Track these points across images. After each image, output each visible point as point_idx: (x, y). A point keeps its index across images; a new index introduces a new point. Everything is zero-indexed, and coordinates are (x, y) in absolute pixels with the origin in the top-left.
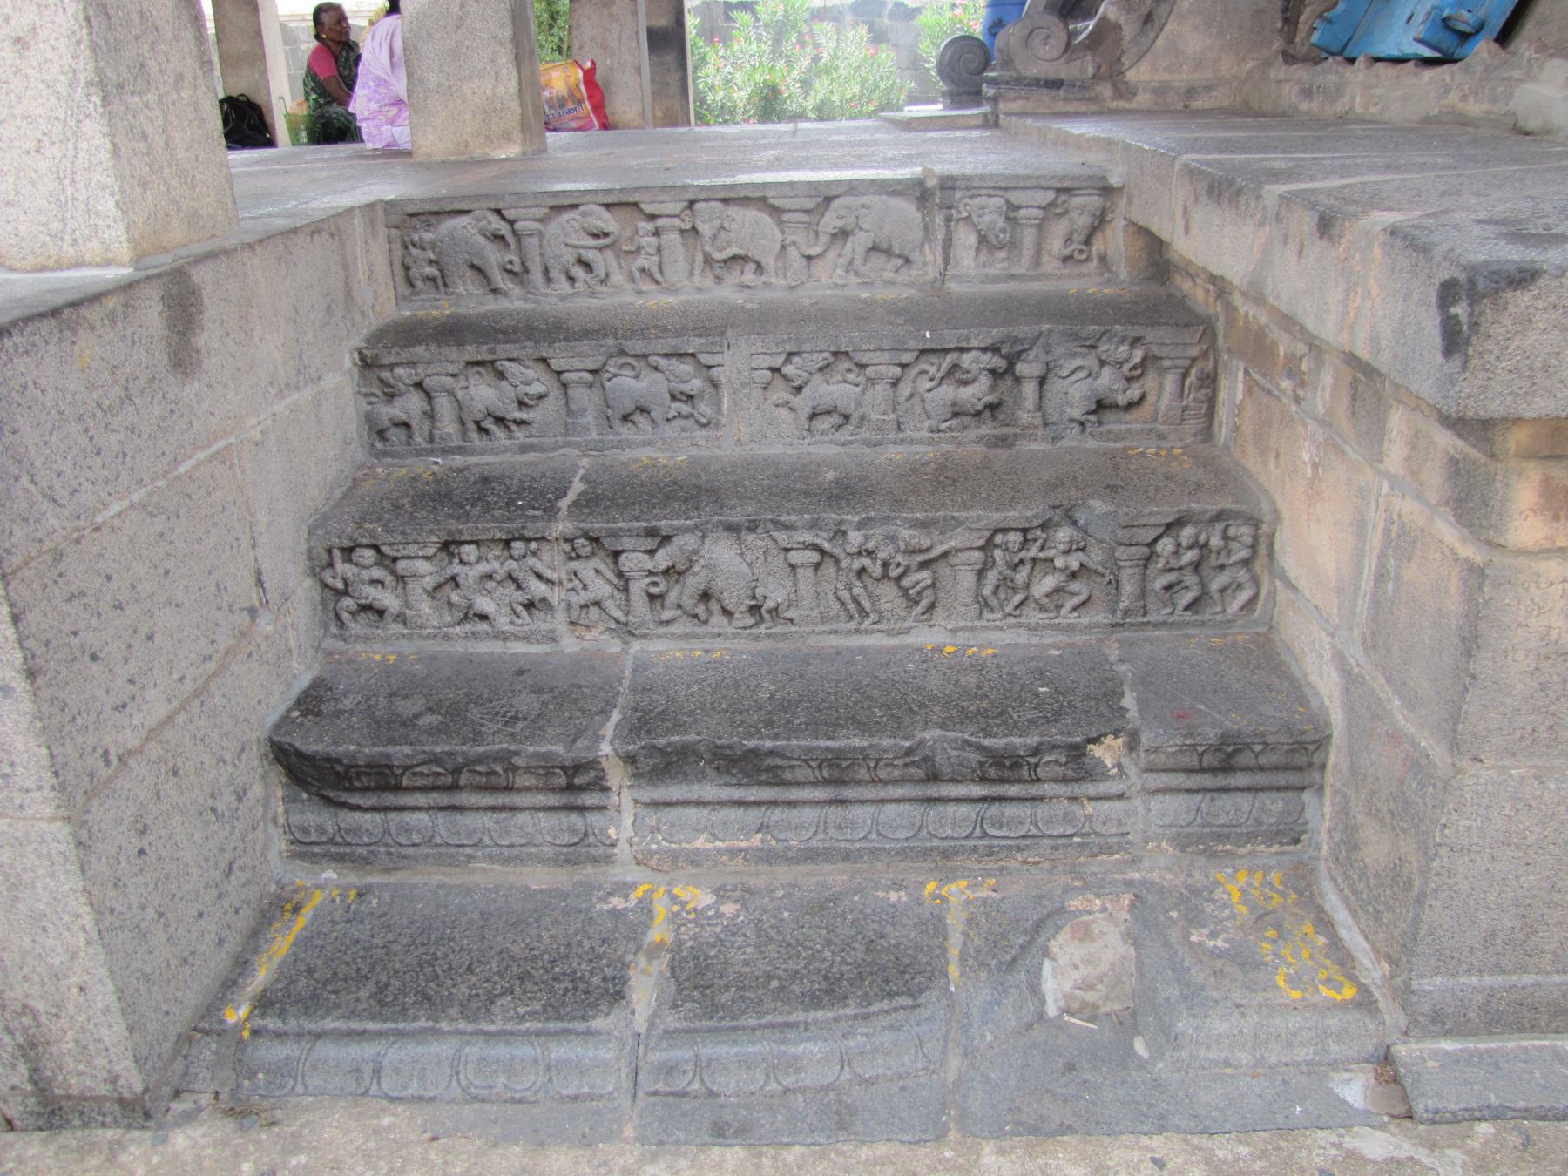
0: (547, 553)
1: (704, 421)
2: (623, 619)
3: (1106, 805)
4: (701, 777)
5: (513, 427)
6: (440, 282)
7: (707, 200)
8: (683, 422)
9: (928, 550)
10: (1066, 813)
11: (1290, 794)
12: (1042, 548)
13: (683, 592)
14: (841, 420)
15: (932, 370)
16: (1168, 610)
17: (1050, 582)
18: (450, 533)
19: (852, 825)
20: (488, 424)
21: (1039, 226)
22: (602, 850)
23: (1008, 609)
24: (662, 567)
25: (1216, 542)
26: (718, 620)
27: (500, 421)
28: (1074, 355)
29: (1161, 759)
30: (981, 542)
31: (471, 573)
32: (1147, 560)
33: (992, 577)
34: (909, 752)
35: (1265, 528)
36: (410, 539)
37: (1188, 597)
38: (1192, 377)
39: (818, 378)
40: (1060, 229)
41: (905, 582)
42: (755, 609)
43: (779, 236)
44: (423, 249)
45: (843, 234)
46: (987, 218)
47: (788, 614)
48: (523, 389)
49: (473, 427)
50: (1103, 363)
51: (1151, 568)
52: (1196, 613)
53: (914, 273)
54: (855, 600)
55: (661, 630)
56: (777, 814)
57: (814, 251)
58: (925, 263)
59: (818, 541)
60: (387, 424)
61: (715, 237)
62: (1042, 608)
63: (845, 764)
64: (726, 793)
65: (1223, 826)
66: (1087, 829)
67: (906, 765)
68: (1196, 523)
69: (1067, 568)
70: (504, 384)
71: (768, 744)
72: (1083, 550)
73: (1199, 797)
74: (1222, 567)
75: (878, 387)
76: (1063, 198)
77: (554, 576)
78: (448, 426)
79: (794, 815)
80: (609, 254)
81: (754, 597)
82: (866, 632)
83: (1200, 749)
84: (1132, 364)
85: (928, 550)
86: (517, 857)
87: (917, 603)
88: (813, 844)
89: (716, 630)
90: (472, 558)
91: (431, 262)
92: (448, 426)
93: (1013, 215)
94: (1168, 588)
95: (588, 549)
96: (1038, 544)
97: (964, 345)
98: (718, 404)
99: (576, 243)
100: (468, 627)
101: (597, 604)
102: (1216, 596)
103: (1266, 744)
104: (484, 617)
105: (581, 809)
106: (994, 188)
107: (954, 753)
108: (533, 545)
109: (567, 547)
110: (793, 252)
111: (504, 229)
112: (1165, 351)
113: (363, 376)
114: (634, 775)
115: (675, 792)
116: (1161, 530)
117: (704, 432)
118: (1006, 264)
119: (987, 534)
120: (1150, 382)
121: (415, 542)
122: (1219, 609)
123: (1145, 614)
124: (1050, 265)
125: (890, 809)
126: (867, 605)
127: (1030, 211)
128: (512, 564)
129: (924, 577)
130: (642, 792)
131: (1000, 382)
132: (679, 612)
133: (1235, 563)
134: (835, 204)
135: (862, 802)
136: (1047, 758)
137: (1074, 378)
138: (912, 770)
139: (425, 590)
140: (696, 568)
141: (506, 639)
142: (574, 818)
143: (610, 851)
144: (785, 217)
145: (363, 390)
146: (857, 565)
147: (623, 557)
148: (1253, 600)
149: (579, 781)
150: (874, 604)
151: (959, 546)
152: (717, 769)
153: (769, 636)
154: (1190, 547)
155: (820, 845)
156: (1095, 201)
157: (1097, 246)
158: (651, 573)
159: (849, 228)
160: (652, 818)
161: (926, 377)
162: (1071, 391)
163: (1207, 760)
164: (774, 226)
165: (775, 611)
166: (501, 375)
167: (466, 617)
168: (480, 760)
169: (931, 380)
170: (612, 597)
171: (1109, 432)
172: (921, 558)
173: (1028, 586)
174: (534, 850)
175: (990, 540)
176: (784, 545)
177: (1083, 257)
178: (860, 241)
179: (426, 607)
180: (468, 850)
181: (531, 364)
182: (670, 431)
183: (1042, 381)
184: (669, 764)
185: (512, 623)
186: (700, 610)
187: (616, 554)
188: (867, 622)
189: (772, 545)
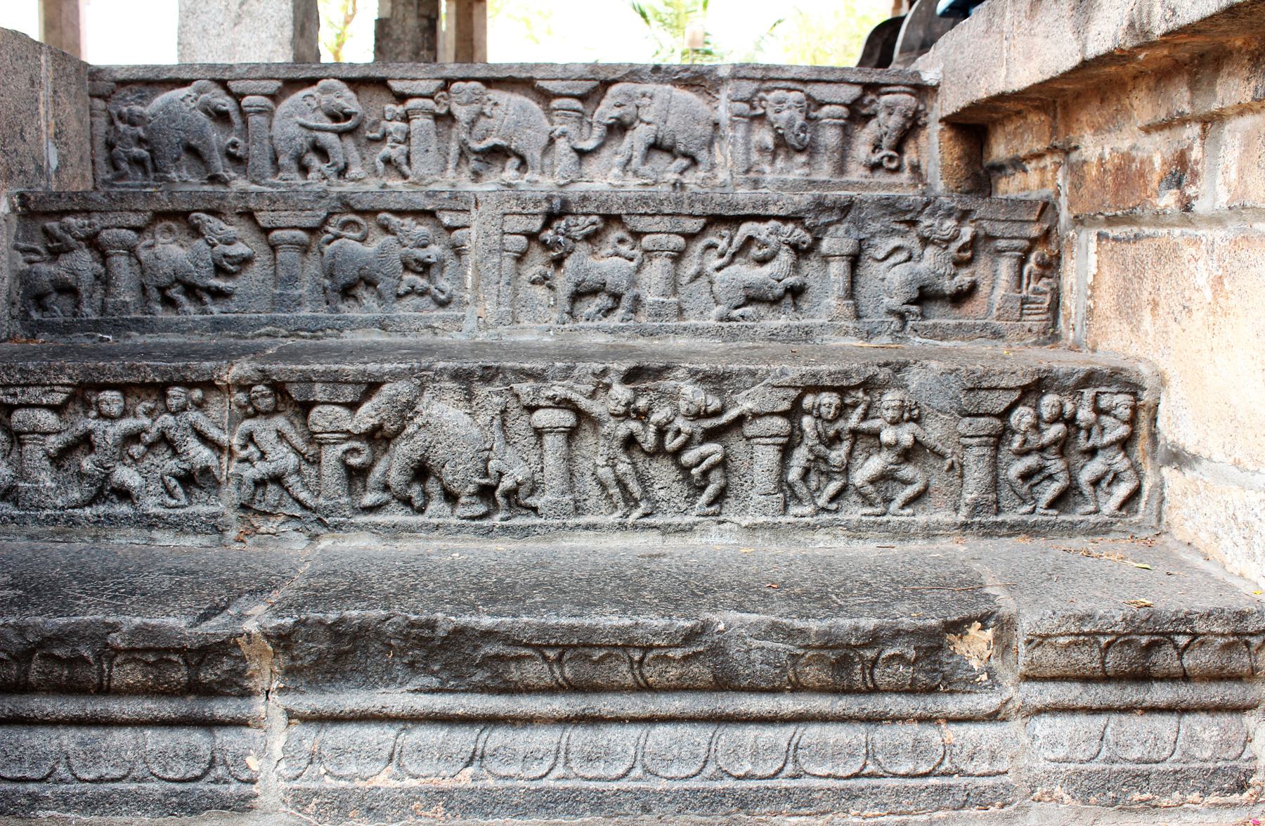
0: (219, 408)
1: (442, 297)
2: (311, 502)
3: (973, 731)
4: (388, 678)
5: (207, 299)
6: (149, 166)
7: (466, 80)
8: (415, 300)
9: (717, 413)
10: (917, 741)
11: (1225, 719)
12: (865, 417)
13: (392, 466)
14: (609, 303)
15: (722, 244)
16: (1027, 508)
17: (875, 464)
18: (86, 372)
19: (607, 755)
20: (174, 293)
21: (844, 127)
22: (233, 787)
23: (822, 502)
24: (363, 427)
25: (1085, 415)
26: (436, 506)
27: (192, 291)
28: (891, 233)
29: (1049, 658)
30: (785, 406)
31: (111, 430)
32: (999, 439)
33: (800, 456)
34: (691, 636)
35: (1146, 397)
36: (32, 380)
37: (1051, 490)
38: (1031, 265)
39: (582, 248)
40: (865, 136)
41: (688, 457)
42: (486, 493)
43: (547, 126)
44: (133, 124)
45: (618, 128)
46: (785, 114)
47: (531, 501)
48: (221, 248)
49: (155, 294)
50: (925, 241)
51: (1004, 449)
52: (1062, 512)
53: (701, 174)
54: (621, 483)
55: (361, 519)
56: (498, 737)
57: (589, 145)
58: (713, 166)
59: (574, 396)
60: (49, 287)
61: (472, 123)
62: (866, 500)
63: (597, 654)
64: (423, 703)
65: (1139, 761)
66: (947, 765)
67: (686, 658)
68: (1060, 390)
69: (897, 443)
70: (200, 243)
71: (487, 622)
72: (917, 420)
73: (1101, 720)
74: (1092, 452)
75: (656, 262)
76: (870, 97)
77: (224, 438)
78: (126, 293)
79: (521, 739)
80: (349, 142)
81: (486, 474)
82: (635, 526)
83: (1104, 641)
84: (959, 243)
85: (717, 413)
86: (106, 796)
87: (703, 489)
88: (548, 783)
89: (435, 521)
90: (115, 409)
91: (140, 141)
92: (126, 293)
93: (813, 114)
94: (1026, 476)
95: (269, 400)
96: (860, 410)
97: (761, 212)
98: (460, 278)
99: (312, 123)
100: (102, 509)
101: (277, 479)
102: (1087, 490)
103: (1195, 635)
104: (124, 494)
105: (210, 724)
106: (793, 80)
107: (756, 643)
108: (197, 394)
109: (241, 397)
110: (562, 145)
111: (226, 103)
112: (999, 229)
113: (27, 234)
114: (289, 672)
115: (352, 700)
116: (1015, 395)
117: (442, 312)
118: (806, 170)
119: (794, 393)
120: (981, 269)
121: (38, 384)
122: (1091, 508)
123: (999, 511)
124: (856, 173)
125: (662, 732)
126: (634, 487)
127: (833, 108)
128: (168, 420)
129: (713, 450)
130: (300, 699)
131: (803, 263)
132: (386, 496)
133: (1112, 444)
134: (614, 89)
135: (619, 720)
136: (889, 652)
137: (892, 260)
138: (695, 668)
139: (47, 453)
140: (410, 429)
141: (151, 526)
142: (197, 738)
143: (246, 789)
144: (556, 103)
145: (22, 245)
146: (623, 429)
147: (314, 413)
148: (1136, 494)
149: (207, 675)
150: (645, 491)
151: (756, 409)
152: (411, 665)
153: (505, 529)
154: (1053, 421)
155: (561, 785)
156: (906, 101)
157: (909, 156)
158: (350, 436)
159: (627, 119)
160: (310, 737)
161: (714, 253)
162: (889, 275)
163: (1112, 659)
164: (541, 114)
165: (510, 494)
166: (196, 232)
167: (100, 491)
168: (61, 637)
169: (722, 256)
170: (298, 471)
171: (935, 326)
172: (708, 424)
173: (846, 470)
174: (134, 786)
175: (797, 402)
176: (526, 400)
177: (894, 165)
178: (638, 137)
179: (46, 479)
180: (32, 787)
181: (235, 219)
182: (404, 310)
183: (855, 261)
184: (339, 656)
185: (162, 505)
186: (415, 491)
187: (306, 407)
188: (636, 514)
189: (513, 403)
